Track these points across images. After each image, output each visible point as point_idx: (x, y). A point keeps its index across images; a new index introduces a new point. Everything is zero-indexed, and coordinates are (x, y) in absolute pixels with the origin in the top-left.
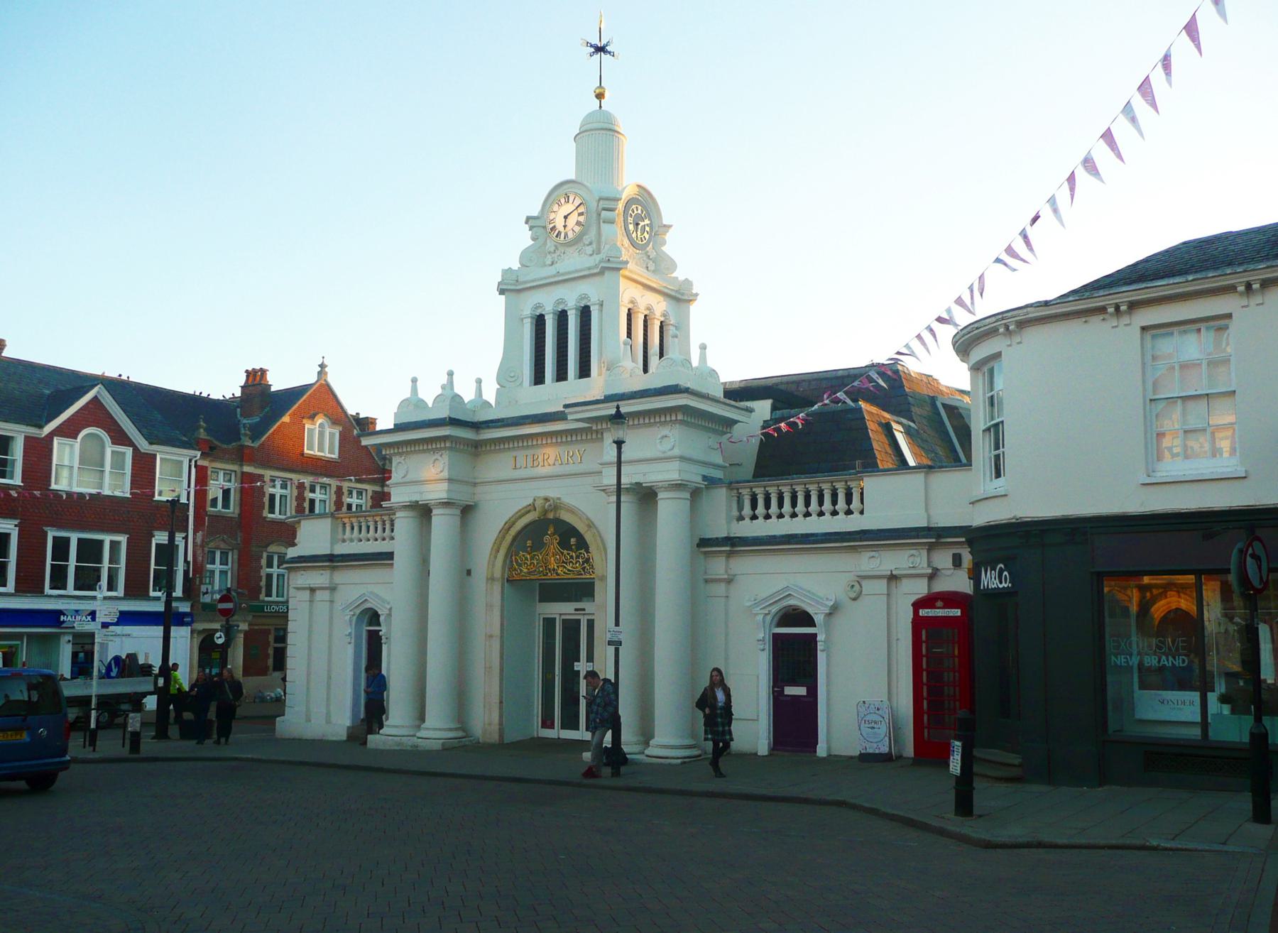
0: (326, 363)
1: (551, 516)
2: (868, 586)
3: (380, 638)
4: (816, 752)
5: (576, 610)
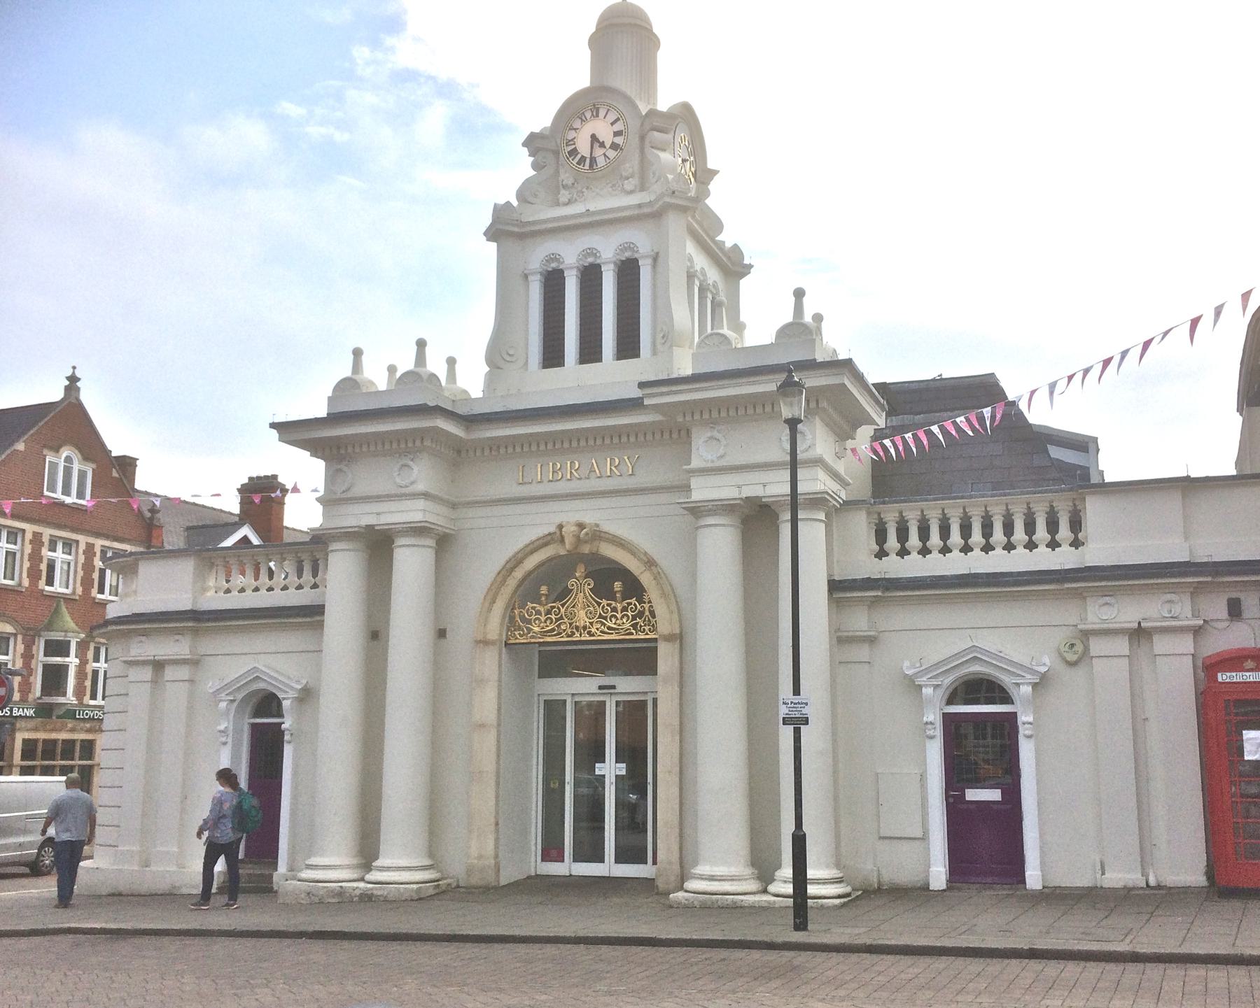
0: (78, 374)
1: (586, 549)
2: (1098, 646)
3: (282, 733)
4: (1024, 882)
5: (600, 688)
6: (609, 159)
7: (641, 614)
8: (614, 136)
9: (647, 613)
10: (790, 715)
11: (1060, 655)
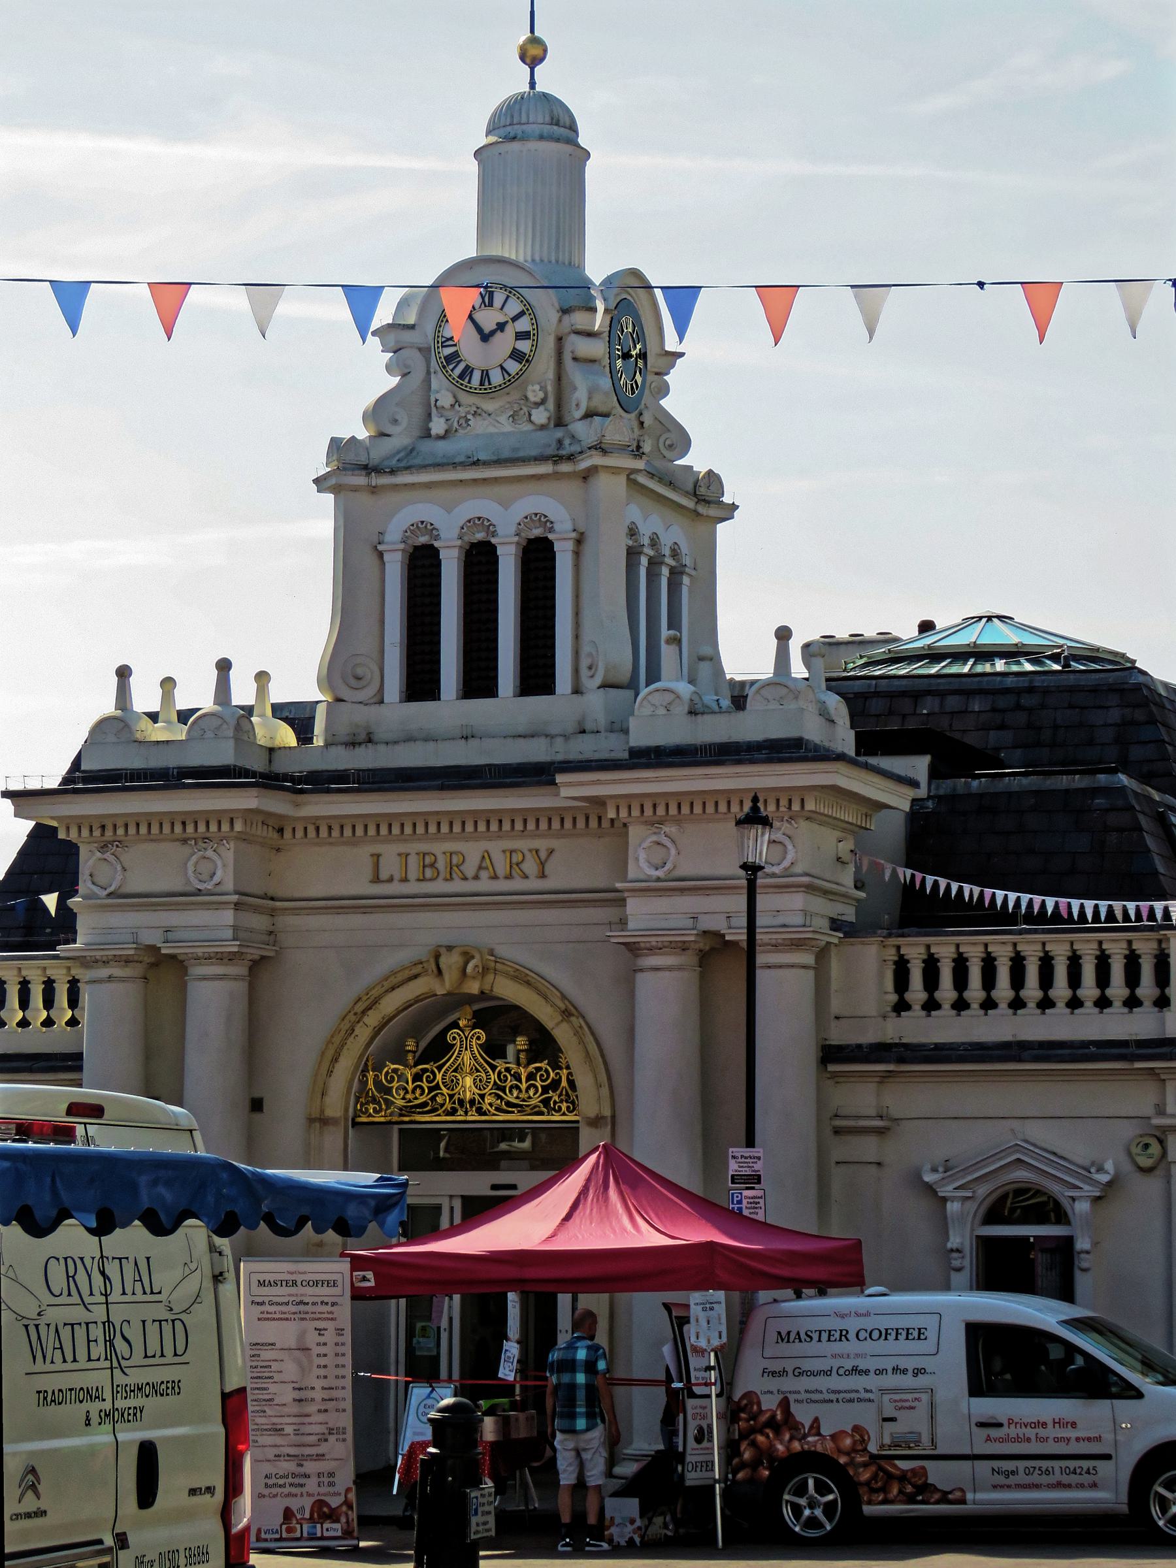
1: (473, 988)
6: (510, 375)
7: (555, 1084)
8: (516, 339)
9: (564, 1083)
10: (740, 1171)
11: (1129, 1154)
